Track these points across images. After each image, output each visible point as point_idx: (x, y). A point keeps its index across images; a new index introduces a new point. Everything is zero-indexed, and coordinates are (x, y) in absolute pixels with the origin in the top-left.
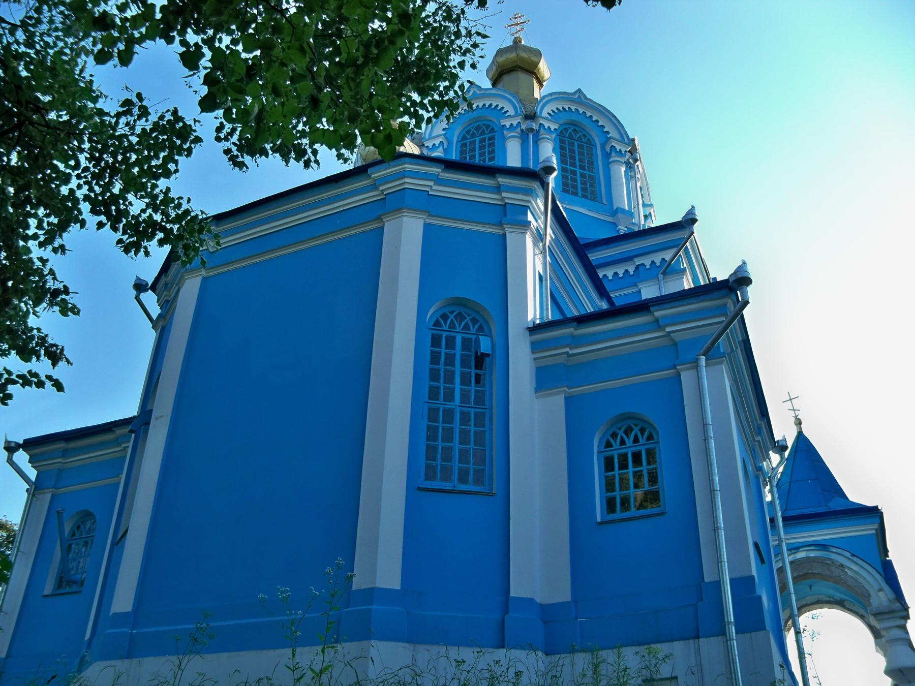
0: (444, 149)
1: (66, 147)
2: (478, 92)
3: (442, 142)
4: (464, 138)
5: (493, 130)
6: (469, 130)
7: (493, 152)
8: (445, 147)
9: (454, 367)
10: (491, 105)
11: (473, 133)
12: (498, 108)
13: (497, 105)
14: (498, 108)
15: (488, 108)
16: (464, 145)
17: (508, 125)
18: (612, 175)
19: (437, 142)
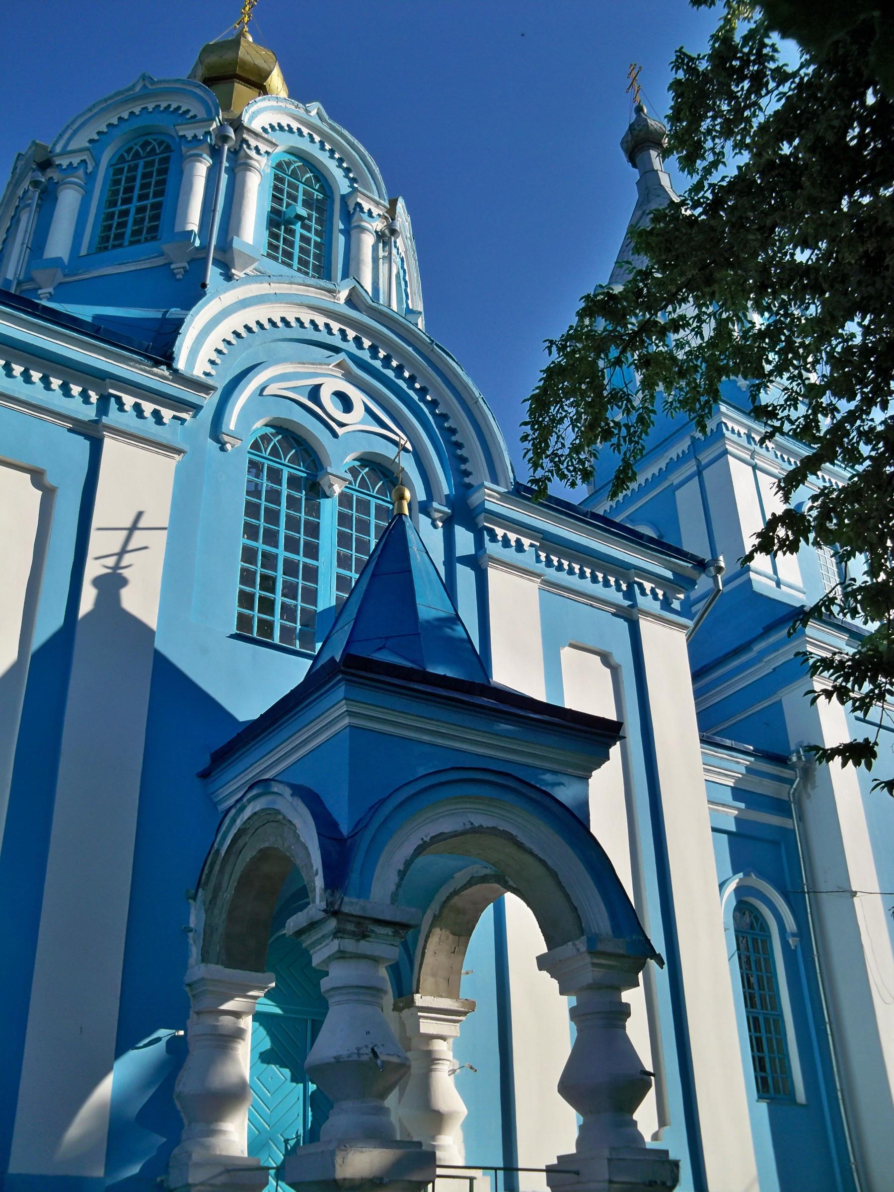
0: (86, 173)
1: (684, 290)
2: (150, 87)
3: (84, 161)
4: (122, 159)
5: (168, 148)
6: (131, 148)
7: (163, 182)
8: (90, 170)
9: (317, 560)
10: (179, 108)
11: (137, 152)
12: (180, 112)
13: (169, 106)
14: (180, 112)
15: (162, 112)
16: (120, 171)
17: (190, 135)
18: (178, 215)
19: (76, 161)
